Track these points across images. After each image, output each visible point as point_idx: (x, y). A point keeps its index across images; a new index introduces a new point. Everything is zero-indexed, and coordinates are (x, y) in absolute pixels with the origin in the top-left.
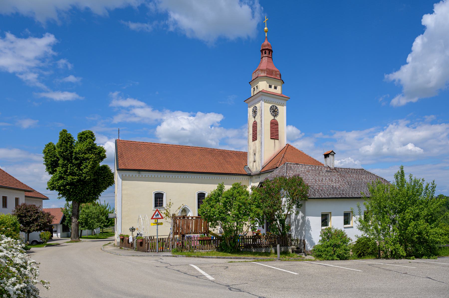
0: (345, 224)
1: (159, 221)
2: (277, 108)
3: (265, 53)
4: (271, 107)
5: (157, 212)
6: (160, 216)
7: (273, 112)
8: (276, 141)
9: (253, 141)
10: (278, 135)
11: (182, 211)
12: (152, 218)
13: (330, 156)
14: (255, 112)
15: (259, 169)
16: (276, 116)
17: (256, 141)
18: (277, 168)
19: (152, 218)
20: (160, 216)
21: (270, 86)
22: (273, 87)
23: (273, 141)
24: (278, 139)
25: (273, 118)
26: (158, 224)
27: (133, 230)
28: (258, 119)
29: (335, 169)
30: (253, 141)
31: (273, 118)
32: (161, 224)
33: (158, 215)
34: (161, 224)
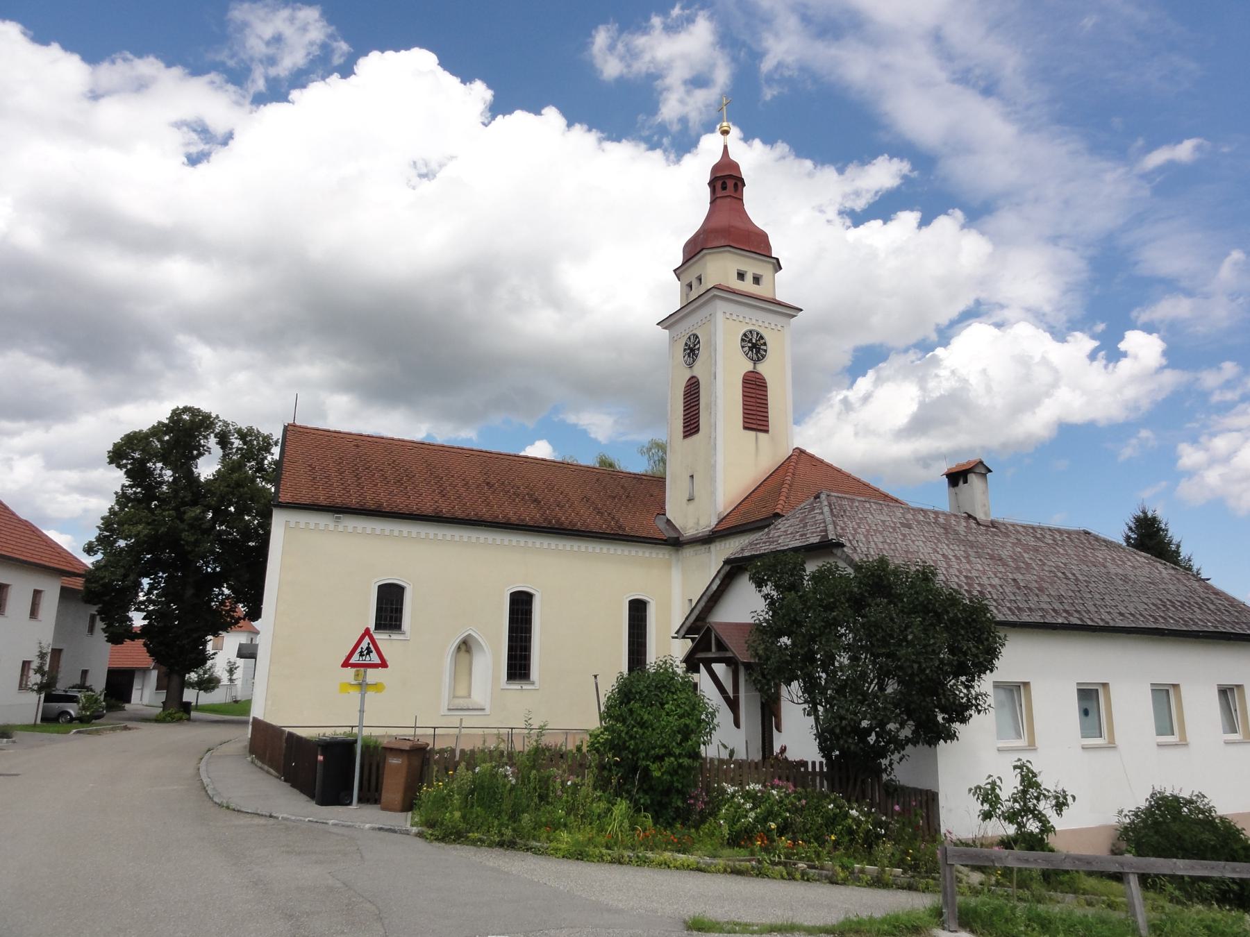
0: (1159, 733)
1: (372, 675)
2: (762, 338)
3: (724, 188)
4: (745, 335)
5: (367, 640)
6: (374, 658)
7: (751, 349)
8: (761, 435)
9: (685, 437)
10: (765, 419)
11: (459, 648)
12: (346, 664)
13: (972, 478)
14: (692, 350)
15: (708, 522)
16: (759, 360)
17: (695, 437)
18: (777, 516)
19: (346, 664)
20: (374, 658)
21: (741, 276)
22: (749, 278)
23: (753, 433)
24: (767, 431)
25: (749, 366)
26: (363, 686)
27: (1121, 812)
28: (699, 370)
29: (993, 524)
30: (685, 437)
31: (749, 366)
32: (377, 687)
33: (369, 652)
34: (377, 687)
